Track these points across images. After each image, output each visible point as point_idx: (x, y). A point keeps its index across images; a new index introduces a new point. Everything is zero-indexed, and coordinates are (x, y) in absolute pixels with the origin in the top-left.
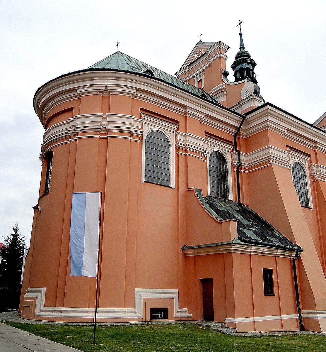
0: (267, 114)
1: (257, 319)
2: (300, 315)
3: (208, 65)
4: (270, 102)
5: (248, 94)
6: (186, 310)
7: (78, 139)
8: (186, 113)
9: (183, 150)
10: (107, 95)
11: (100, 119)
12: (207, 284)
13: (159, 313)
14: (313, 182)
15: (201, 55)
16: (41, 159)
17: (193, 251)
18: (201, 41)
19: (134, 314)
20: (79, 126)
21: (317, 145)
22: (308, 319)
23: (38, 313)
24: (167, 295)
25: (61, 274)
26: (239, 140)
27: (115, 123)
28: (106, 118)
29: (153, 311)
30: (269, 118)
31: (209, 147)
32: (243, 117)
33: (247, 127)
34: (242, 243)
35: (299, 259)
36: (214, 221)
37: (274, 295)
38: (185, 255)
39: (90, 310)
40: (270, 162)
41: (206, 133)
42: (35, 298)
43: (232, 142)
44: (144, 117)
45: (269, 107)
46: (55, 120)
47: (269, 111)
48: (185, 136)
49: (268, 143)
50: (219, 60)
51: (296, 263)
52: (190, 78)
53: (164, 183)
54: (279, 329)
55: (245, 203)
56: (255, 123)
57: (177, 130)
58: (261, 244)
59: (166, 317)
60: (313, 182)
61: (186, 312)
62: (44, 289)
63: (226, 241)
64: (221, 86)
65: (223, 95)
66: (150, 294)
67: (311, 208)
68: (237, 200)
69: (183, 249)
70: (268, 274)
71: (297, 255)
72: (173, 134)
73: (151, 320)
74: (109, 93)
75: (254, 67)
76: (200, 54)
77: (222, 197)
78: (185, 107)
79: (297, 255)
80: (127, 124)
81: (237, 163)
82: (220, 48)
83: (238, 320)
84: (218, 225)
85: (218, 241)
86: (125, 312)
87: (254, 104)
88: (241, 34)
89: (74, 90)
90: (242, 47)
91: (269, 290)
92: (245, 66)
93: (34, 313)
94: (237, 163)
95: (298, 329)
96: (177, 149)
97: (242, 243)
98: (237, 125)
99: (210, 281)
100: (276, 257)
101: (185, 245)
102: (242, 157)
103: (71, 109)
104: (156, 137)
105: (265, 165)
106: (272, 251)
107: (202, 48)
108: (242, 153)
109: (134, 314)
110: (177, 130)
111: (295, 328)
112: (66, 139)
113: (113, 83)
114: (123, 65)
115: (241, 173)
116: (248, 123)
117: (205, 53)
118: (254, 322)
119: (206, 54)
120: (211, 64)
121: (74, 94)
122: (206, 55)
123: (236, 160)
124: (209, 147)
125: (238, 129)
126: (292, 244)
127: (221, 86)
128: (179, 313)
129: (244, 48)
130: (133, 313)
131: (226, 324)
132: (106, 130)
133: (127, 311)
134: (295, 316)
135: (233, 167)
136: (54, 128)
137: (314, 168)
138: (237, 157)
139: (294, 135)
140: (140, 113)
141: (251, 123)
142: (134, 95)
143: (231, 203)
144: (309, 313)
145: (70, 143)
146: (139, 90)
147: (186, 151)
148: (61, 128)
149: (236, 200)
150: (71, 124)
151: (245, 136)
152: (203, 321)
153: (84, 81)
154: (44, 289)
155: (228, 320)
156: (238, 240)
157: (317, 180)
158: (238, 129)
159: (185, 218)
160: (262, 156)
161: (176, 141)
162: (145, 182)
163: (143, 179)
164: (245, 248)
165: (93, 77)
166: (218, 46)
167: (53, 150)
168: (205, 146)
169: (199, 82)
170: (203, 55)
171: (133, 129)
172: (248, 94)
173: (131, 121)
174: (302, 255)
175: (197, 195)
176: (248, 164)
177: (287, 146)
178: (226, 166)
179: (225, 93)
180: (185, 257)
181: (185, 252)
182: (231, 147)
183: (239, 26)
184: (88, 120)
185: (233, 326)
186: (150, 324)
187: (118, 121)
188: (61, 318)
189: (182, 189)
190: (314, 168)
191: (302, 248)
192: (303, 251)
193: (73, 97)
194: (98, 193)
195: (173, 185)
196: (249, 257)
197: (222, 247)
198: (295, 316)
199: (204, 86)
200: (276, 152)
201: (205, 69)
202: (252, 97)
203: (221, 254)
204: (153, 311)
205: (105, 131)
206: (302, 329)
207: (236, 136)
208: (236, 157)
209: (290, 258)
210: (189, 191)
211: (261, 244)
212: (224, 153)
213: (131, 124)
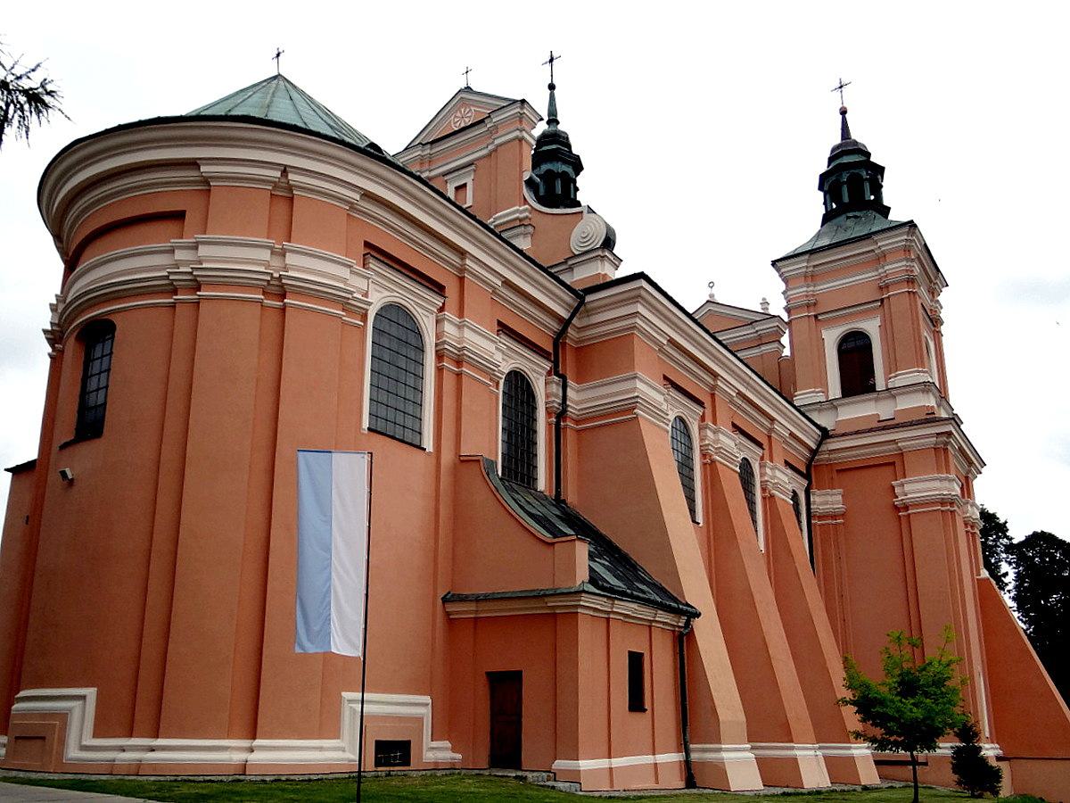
0: (636, 297)
1: (617, 762)
2: (688, 755)
3: (485, 152)
4: (646, 273)
5: (589, 243)
6: (447, 744)
7: (202, 298)
8: (462, 269)
9: (455, 360)
10: (284, 194)
11: (265, 255)
12: (505, 688)
13: (393, 752)
14: (705, 464)
15: (469, 122)
16: (51, 337)
17: (472, 607)
18: (468, 88)
19: (339, 755)
20: (204, 266)
21: (719, 383)
22: (703, 764)
23: (73, 753)
24: (403, 708)
25: (150, 653)
26: (568, 350)
27: (232, 262)
28: (283, 253)
29: (381, 746)
30: (640, 309)
31: (503, 358)
32: (580, 295)
33: (585, 322)
34: (598, 591)
35: (691, 635)
36: (532, 541)
37: (644, 710)
38: (448, 614)
39: (233, 745)
40: (635, 411)
41: (500, 323)
42: (64, 717)
43: (549, 354)
44: (373, 264)
45: (644, 283)
46: (118, 236)
47: (643, 293)
48: (460, 327)
49: (632, 368)
50: (518, 146)
51: (684, 642)
52: (433, 173)
53: (409, 436)
54: (651, 785)
55: (569, 501)
56: (605, 317)
57: (441, 309)
58: (623, 594)
59: (406, 762)
60: (705, 464)
61: (447, 749)
62: (91, 692)
63: (564, 586)
64: (521, 212)
65: (525, 235)
66: (385, 707)
67: (698, 523)
68: (554, 493)
69: (445, 600)
70: (636, 661)
71: (688, 624)
72: (432, 319)
73: (380, 769)
74: (290, 188)
75: (577, 174)
76: (467, 120)
77: (524, 483)
78: (462, 253)
79: (688, 624)
80: (333, 277)
81: (559, 404)
82: (521, 116)
83: (584, 764)
84: (544, 549)
85: (544, 585)
86: (321, 749)
87: (603, 269)
88: (552, 87)
89: (193, 164)
90: (553, 120)
91: (636, 704)
92: (560, 167)
93: (61, 754)
94: (559, 404)
95: (682, 784)
96: (440, 356)
97: (598, 591)
98: (565, 314)
99: (517, 676)
100: (650, 627)
101: (449, 593)
102: (570, 392)
103: (179, 216)
104: (394, 316)
105: (624, 415)
106: (646, 613)
107: (474, 106)
108: (570, 382)
109: (339, 755)
110: (441, 309)
111: (676, 781)
112: (166, 295)
113: (308, 167)
114: (309, 116)
115: (566, 427)
116: (589, 313)
117: (482, 121)
118: (611, 769)
119: (472, 120)
120: (495, 150)
121: (190, 174)
122: (483, 124)
123: (556, 396)
124: (503, 358)
125: (566, 323)
126: (675, 600)
127: (521, 212)
128: (434, 752)
129: (558, 123)
130: (334, 752)
131: (555, 774)
132: (282, 286)
133: (325, 745)
134: (675, 757)
135: (549, 413)
136: (116, 259)
137: (709, 433)
138: (558, 390)
139: (706, 355)
140: (364, 255)
141: (597, 314)
142: (352, 206)
143: (540, 497)
144: (704, 750)
145: (173, 306)
146: (367, 195)
147: (459, 363)
148: (136, 262)
149: (551, 491)
150: (180, 255)
151: (576, 342)
152: (489, 769)
153: (277, 151)
154: (91, 692)
155: (559, 764)
156: (590, 586)
157: (713, 462)
158: (566, 323)
159: (453, 526)
160: (608, 396)
161: (438, 337)
162: (369, 429)
163: (366, 424)
164: (601, 603)
165: (271, 143)
166: (518, 110)
167: (116, 319)
168: (498, 357)
169: (457, 189)
170: (473, 125)
171: (351, 293)
172: (589, 243)
173: (345, 273)
174: (697, 624)
175: (488, 475)
176: (579, 410)
177: (665, 378)
178: (534, 408)
179: (530, 229)
180: (450, 621)
181: (451, 608)
182: (548, 366)
183: (548, 65)
184: (232, 252)
185: (575, 777)
186: (391, 776)
187: (312, 265)
188: (154, 766)
189: (447, 457)
190: (709, 433)
191: (700, 609)
192: (700, 614)
193: (188, 182)
194: (362, 455)
195: (428, 444)
196: (605, 624)
197: (552, 599)
198: (675, 757)
199: (471, 201)
200: (648, 389)
201: (477, 159)
202: (600, 253)
203: (548, 616)
204: (381, 746)
205: (279, 289)
206: (690, 782)
207: (559, 339)
208: (556, 389)
209: (674, 631)
210: (464, 461)
211: (623, 594)
212: (532, 376)
213: (345, 281)
